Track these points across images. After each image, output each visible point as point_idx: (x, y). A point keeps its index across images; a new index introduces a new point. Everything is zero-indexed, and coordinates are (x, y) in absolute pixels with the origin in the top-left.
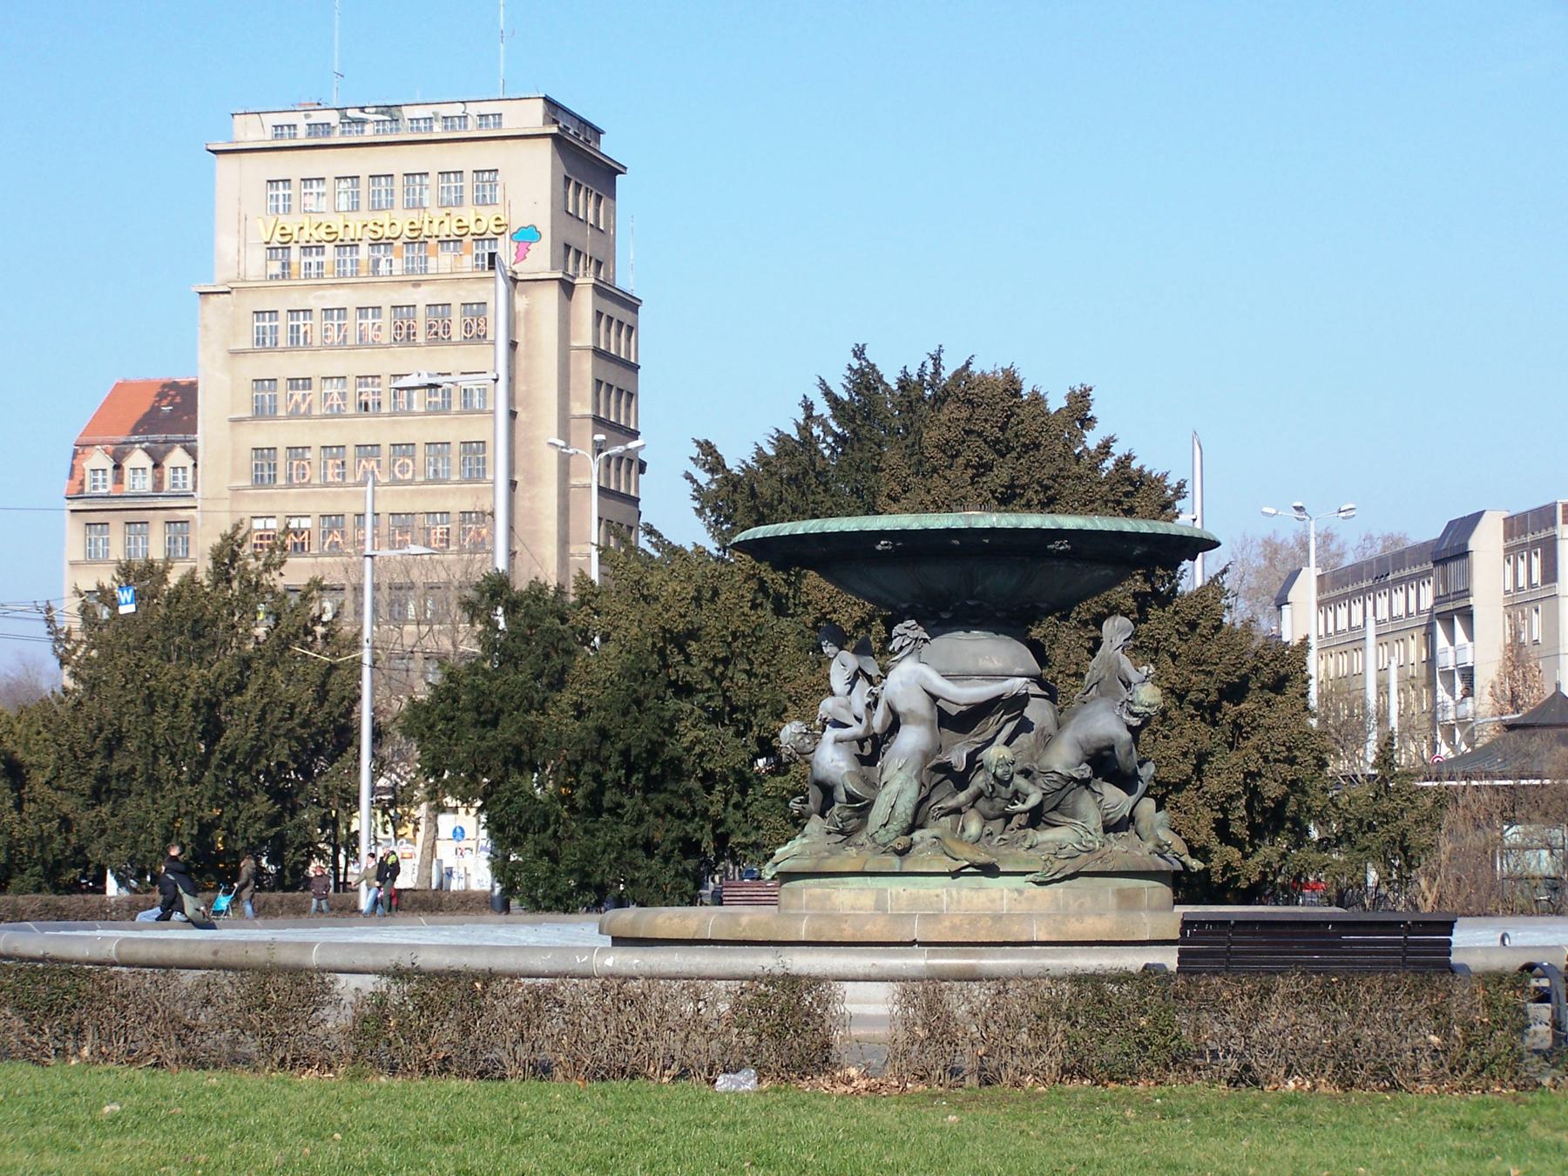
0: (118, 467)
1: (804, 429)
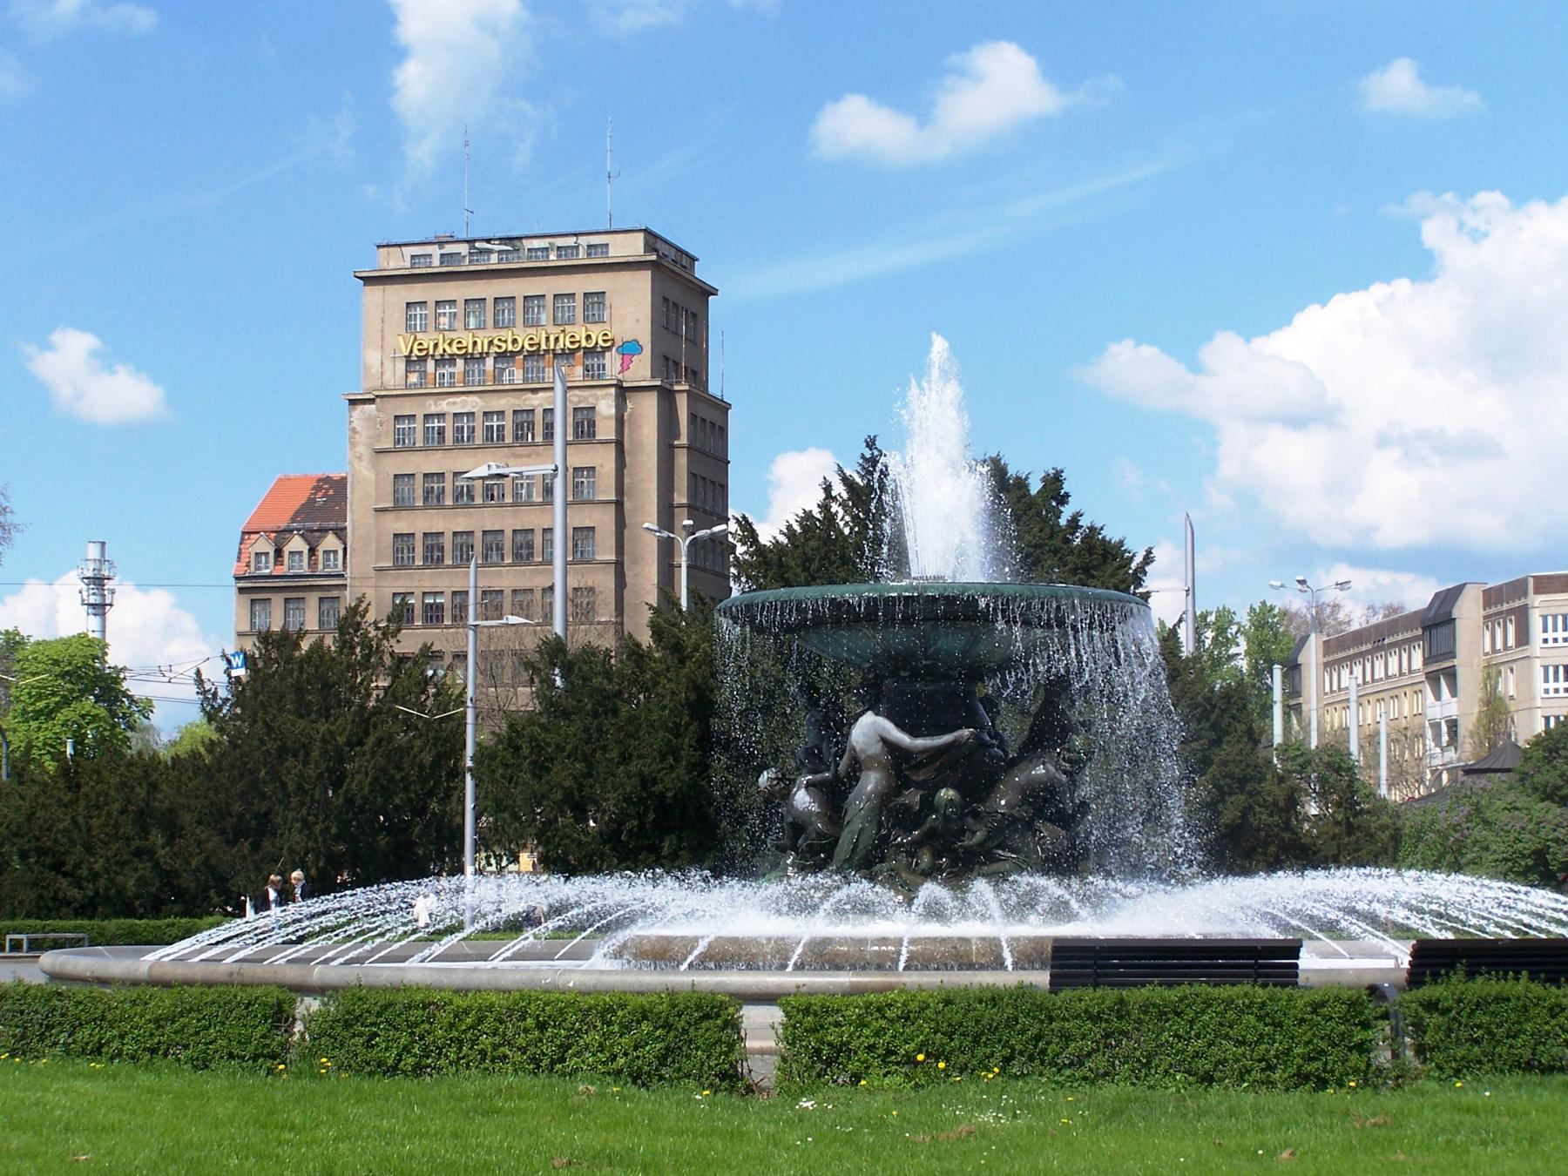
0: (312, 551)
1: (825, 507)
